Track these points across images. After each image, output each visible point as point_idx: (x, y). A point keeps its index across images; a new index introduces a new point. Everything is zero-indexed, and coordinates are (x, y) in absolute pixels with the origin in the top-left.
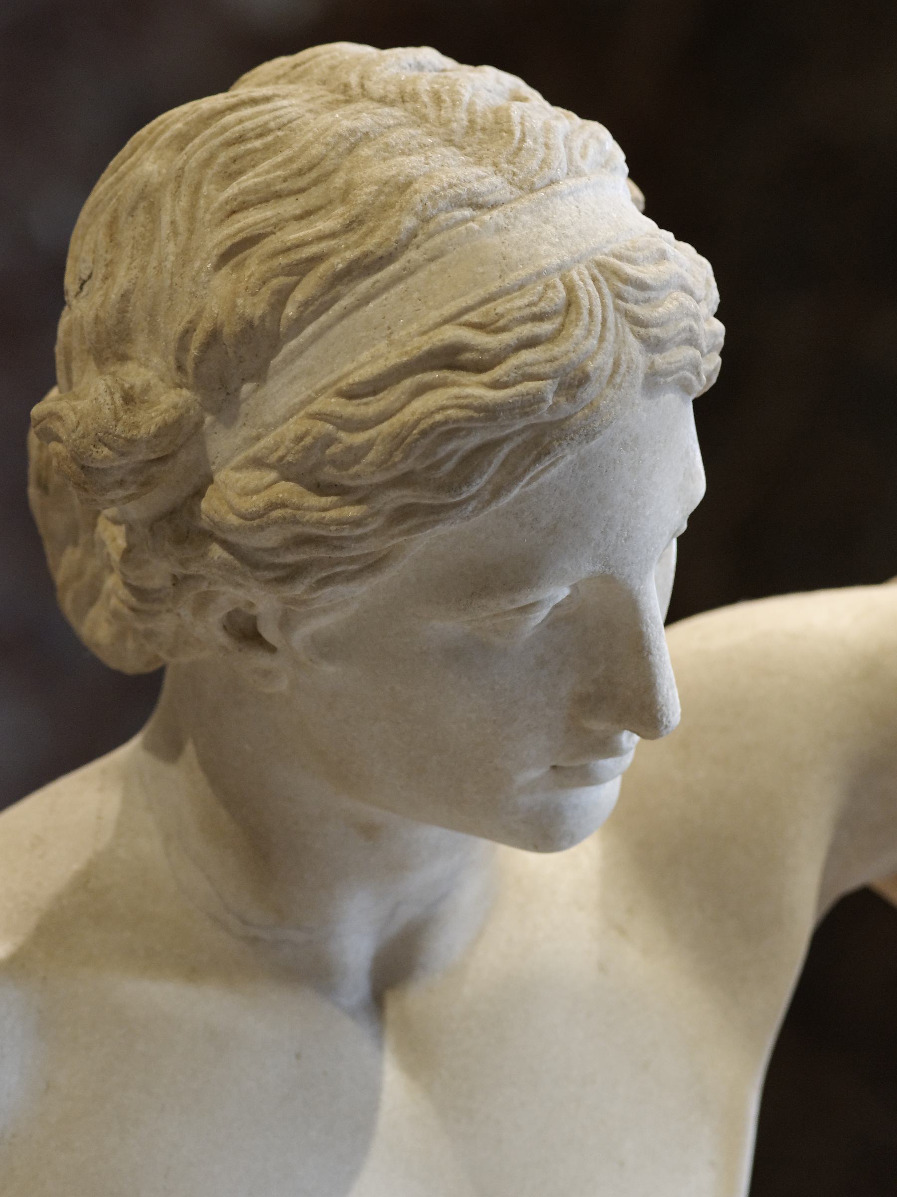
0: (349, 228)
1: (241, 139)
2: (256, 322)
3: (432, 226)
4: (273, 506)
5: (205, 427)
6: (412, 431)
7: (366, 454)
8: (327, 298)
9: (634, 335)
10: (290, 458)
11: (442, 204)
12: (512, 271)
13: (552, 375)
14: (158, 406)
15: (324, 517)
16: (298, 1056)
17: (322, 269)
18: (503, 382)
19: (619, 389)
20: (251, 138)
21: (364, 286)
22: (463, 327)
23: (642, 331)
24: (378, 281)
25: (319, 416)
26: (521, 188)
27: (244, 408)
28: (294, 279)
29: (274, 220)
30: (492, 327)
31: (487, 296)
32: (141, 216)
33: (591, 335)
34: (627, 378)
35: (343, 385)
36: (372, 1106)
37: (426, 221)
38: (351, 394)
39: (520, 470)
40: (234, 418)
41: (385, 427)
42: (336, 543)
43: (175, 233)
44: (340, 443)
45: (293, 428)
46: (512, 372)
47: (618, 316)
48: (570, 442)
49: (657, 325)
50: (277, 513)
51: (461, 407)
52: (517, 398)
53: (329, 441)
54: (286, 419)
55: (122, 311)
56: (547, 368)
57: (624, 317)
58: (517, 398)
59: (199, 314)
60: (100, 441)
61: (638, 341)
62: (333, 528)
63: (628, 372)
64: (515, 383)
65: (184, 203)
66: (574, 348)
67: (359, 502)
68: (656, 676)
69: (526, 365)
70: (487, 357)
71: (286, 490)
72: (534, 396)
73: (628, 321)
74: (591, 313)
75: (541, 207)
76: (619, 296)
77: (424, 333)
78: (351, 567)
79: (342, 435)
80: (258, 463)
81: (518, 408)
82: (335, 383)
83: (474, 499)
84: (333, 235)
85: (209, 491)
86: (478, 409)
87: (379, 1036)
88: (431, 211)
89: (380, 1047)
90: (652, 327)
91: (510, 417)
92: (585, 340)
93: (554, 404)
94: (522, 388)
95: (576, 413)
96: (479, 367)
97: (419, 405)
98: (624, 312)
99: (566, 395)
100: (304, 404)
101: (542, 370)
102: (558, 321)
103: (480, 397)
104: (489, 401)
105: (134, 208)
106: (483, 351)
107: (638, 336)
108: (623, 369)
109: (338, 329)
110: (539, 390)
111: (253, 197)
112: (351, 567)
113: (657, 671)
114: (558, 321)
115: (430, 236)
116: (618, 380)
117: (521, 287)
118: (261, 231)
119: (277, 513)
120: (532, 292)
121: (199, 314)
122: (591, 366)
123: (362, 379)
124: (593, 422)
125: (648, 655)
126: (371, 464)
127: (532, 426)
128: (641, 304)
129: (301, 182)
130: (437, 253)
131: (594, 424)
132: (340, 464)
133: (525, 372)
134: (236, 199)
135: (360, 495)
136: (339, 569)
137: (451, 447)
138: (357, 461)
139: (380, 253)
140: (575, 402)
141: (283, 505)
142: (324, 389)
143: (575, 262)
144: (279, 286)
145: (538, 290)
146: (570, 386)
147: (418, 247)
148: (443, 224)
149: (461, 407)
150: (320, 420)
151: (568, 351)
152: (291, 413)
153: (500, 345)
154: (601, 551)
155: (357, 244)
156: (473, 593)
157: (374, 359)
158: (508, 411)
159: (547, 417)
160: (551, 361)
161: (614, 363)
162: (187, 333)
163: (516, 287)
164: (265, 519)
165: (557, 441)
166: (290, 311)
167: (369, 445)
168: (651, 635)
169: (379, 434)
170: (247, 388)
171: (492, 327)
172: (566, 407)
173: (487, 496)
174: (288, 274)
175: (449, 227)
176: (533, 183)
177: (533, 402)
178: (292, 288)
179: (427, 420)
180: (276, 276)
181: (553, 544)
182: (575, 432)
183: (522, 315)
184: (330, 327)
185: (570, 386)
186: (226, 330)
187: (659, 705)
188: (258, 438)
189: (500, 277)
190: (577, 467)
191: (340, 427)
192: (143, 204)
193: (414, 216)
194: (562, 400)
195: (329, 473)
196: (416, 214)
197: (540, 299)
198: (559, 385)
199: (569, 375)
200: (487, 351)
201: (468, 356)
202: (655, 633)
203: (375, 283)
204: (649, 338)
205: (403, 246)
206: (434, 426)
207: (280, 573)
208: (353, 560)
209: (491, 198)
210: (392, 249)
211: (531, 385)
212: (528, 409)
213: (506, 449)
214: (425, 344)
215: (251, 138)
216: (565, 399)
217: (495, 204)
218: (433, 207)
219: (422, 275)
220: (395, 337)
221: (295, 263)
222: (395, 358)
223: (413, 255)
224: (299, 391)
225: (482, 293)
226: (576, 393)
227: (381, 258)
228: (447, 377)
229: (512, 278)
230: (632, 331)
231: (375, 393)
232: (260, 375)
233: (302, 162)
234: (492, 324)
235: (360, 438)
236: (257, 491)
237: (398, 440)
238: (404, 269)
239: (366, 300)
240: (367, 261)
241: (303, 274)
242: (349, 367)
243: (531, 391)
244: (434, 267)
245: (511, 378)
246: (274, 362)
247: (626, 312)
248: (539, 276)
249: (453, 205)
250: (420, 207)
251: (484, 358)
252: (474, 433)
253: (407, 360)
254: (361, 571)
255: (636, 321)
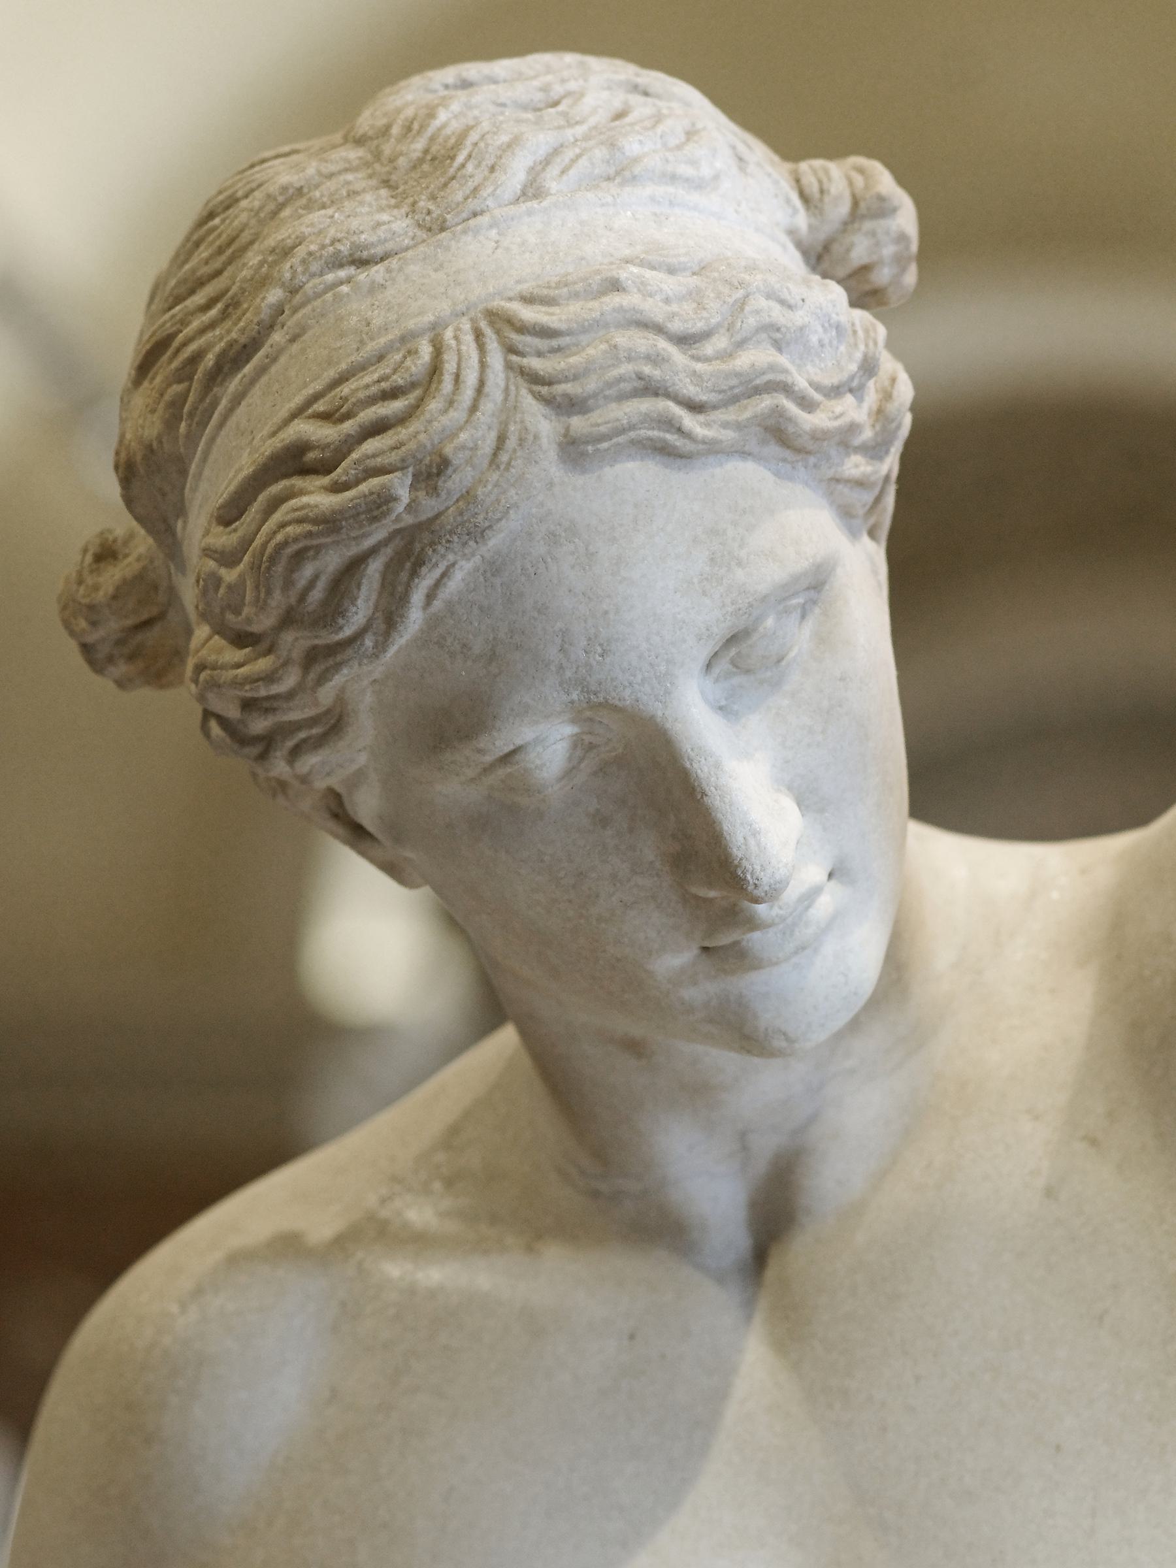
0: (225, 315)
3: (298, 298)
9: (535, 397)
11: (315, 267)
12: (372, 339)
13: (399, 465)
14: (253, 544)
15: (237, 675)
16: (632, 1337)
18: (342, 483)
19: (507, 469)
21: (234, 385)
22: (311, 420)
23: (544, 390)
26: (430, 230)
31: (337, 376)
33: (452, 407)
34: (519, 454)
36: (719, 1396)
37: (294, 291)
39: (400, 589)
42: (266, 704)
46: (351, 469)
47: (511, 375)
48: (448, 545)
49: (566, 380)
51: (299, 521)
52: (358, 501)
56: (393, 458)
57: (520, 376)
58: (358, 501)
61: (541, 404)
62: (247, 687)
63: (520, 445)
64: (357, 482)
65: (209, 335)
66: (426, 427)
68: (720, 822)
69: (368, 457)
72: (379, 495)
73: (525, 380)
74: (457, 378)
75: (439, 250)
76: (511, 349)
78: (316, 731)
81: (363, 513)
83: (367, 632)
86: (315, 521)
87: (749, 1306)
88: (301, 278)
89: (749, 1318)
90: (559, 382)
91: (356, 525)
92: (442, 415)
93: (413, 501)
94: (364, 488)
95: (448, 508)
98: (519, 371)
99: (426, 487)
101: (386, 461)
102: (417, 393)
103: (316, 506)
104: (324, 509)
106: (324, 447)
107: (539, 397)
108: (511, 443)
110: (383, 486)
112: (316, 731)
113: (719, 816)
114: (417, 393)
115: (295, 311)
116: (504, 457)
117: (381, 358)
118: (171, 331)
120: (386, 363)
122: (448, 450)
124: (474, 517)
125: (702, 798)
127: (397, 532)
128: (549, 355)
129: (217, 264)
130: (297, 331)
131: (476, 518)
133: (366, 466)
136: (302, 735)
137: (308, 571)
139: (243, 340)
140: (438, 495)
143: (457, 315)
144: (171, 397)
145: (395, 359)
146: (429, 476)
147: (283, 327)
148: (310, 293)
149: (299, 521)
151: (418, 433)
153: (339, 436)
154: (568, 674)
158: (352, 519)
159: (409, 520)
160: (397, 448)
161: (499, 437)
163: (375, 359)
165: (431, 547)
168: (699, 771)
171: (337, 415)
172: (430, 506)
173: (379, 624)
174: (180, 381)
175: (318, 296)
176: (445, 221)
177: (381, 503)
178: (184, 396)
181: (500, 674)
182: (451, 532)
183: (368, 394)
185: (429, 476)
187: (736, 859)
189: (358, 349)
190: (489, 575)
193: (280, 288)
194: (421, 494)
196: (283, 285)
197: (395, 371)
198: (414, 475)
199: (424, 462)
200: (328, 445)
201: (311, 456)
202: (706, 770)
203: (242, 378)
204: (554, 397)
205: (270, 327)
208: (313, 721)
209: (379, 251)
210: (254, 333)
211: (375, 482)
212: (375, 513)
213: (375, 567)
214: (270, 446)
216: (424, 493)
217: (385, 255)
218: (304, 273)
223: (277, 337)
225: (331, 374)
226: (437, 483)
227: (245, 346)
228: (293, 486)
229: (372, 347)
230: (532, 392)
234: (338, 410)
240: (232, 353)
243: (374, 490)
244: (295, 347)
245: (351, 477)
246: (187, 491)
247: (521, 370)
248: (404, 342)
249: (330, 266)
250: (288, 275)
251: (325, 455)
252: (324, 551)
253: (253, 471)
255: (534, 379)
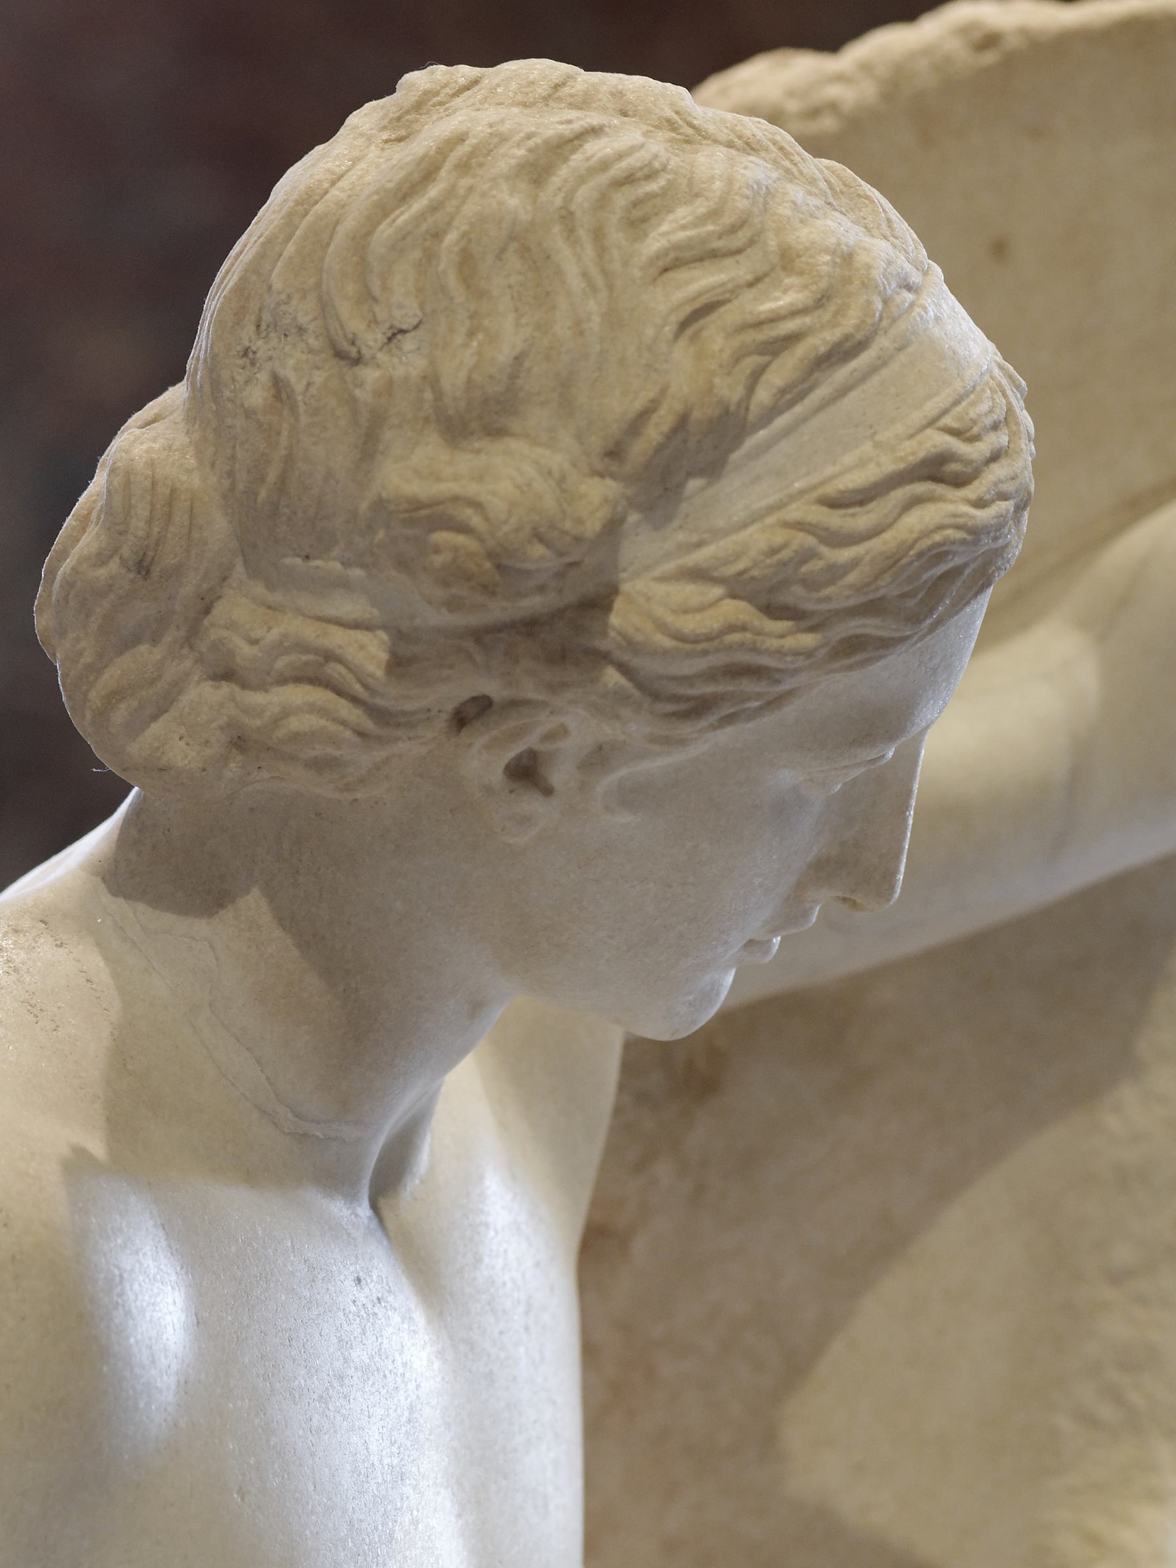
1: (629, 179)
2: (733, 408)
4: (732, 628)
5: (626, 526)
6: (909, 551)
7: (845, 574)
8: (806, 385)
10: (755, 573)
17: (801, 351)
20: (639, 179)
21: (842, 374)
24: (855, 370)
25: (800, 526)
27: (684, 507)
28: (767, 358)
29: (730, 286)
30: (968, 435)
32: (513, 261)
35: (830, 490)
38: (834, 503)
40: (668, 519)
41: (876, 544)
43: (594, 289)
44: (820, 559)
45: (757, 538)
50: (736, 637)
51: (958, 527)
53: (807, 555)
54: (744, 525)
55: (513, 377)
59: (663, 391)
60: (538, 536)
65: (589, 252)
67: (812, 629)
70: (969, 470)
71: (738, 610)
77: (911, 436)
79: (824, 550)
80: (698, 575)
82: (814, 488)
84: (803, 311)
85: (618, 604)
96: (959, 482)
97: (915, 521)
100: (772, 509)
105: (503, 250)
109: (815, 423)
111: (688, 254)
119: (736, 637)
121: (663, 391)
123: (851, 486)
126: (851, 586)
132: (811, 584)
134: (667, 255)
135: (814, 621)
138: (831, 582)
141: (743, 628)
142: (802, 493)
150: (801, 530)
152: (755, 518)
155: (833, 324)
156: (854, 741)
157: (862, 463)
160: (1013, 479)
162: (645, 414)
164: (716, 642)
166: (763, 395)
167: (855, 563)
169: (867, 553)
170: (693, 484)
179: (925, 540)
180: (750, 354)
184: (804, 419)
186: (697, 414)
188: (699, 545)
191: (823, 541)
192: (513, 246)
195: (796, 595)
200: (971, 462)
201: (953, 467)
206: (920, 555)
207: (683, 707)
215: (639, 179)
219: (894, 366)
220: (878, 438)
221: (771, 340)
222: (888, 465)
224: (765, 494)
231: (861, 503)
232: (713, 469)
233: (728, 220)
235: (845, 555)
236: (701, 609)
237: (891, 562)
238: (879, 358)
239: (843, 392)
240: (848, 345)
241: (775, 354)
242: (829, 470)
246: (735, 456)
254: (761, 708)
